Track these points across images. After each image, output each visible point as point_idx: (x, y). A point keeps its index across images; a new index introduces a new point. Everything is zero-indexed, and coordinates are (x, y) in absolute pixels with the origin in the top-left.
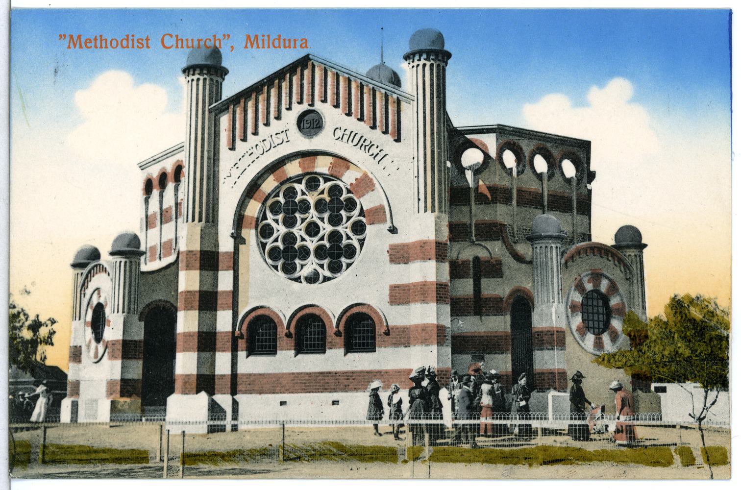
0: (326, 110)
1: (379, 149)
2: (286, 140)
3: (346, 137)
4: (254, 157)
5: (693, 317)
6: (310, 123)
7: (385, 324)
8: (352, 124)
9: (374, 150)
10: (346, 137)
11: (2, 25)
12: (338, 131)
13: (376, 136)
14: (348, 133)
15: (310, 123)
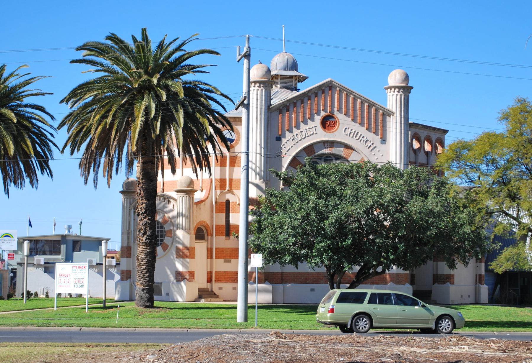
0: (340, 116)
1: (372, 143)
2: (315, 132)
3: (352, 134)
4: (296, 141)
5: (136, 119)
6: (328, 122)
7: (118, 135)
8: (356, 127)
9: (369, 144)
10: (352, 134)
11: (69, 228)
12: (347, 130)
13: (370, 136)
14: (353, 131)
15: (328, 122)
